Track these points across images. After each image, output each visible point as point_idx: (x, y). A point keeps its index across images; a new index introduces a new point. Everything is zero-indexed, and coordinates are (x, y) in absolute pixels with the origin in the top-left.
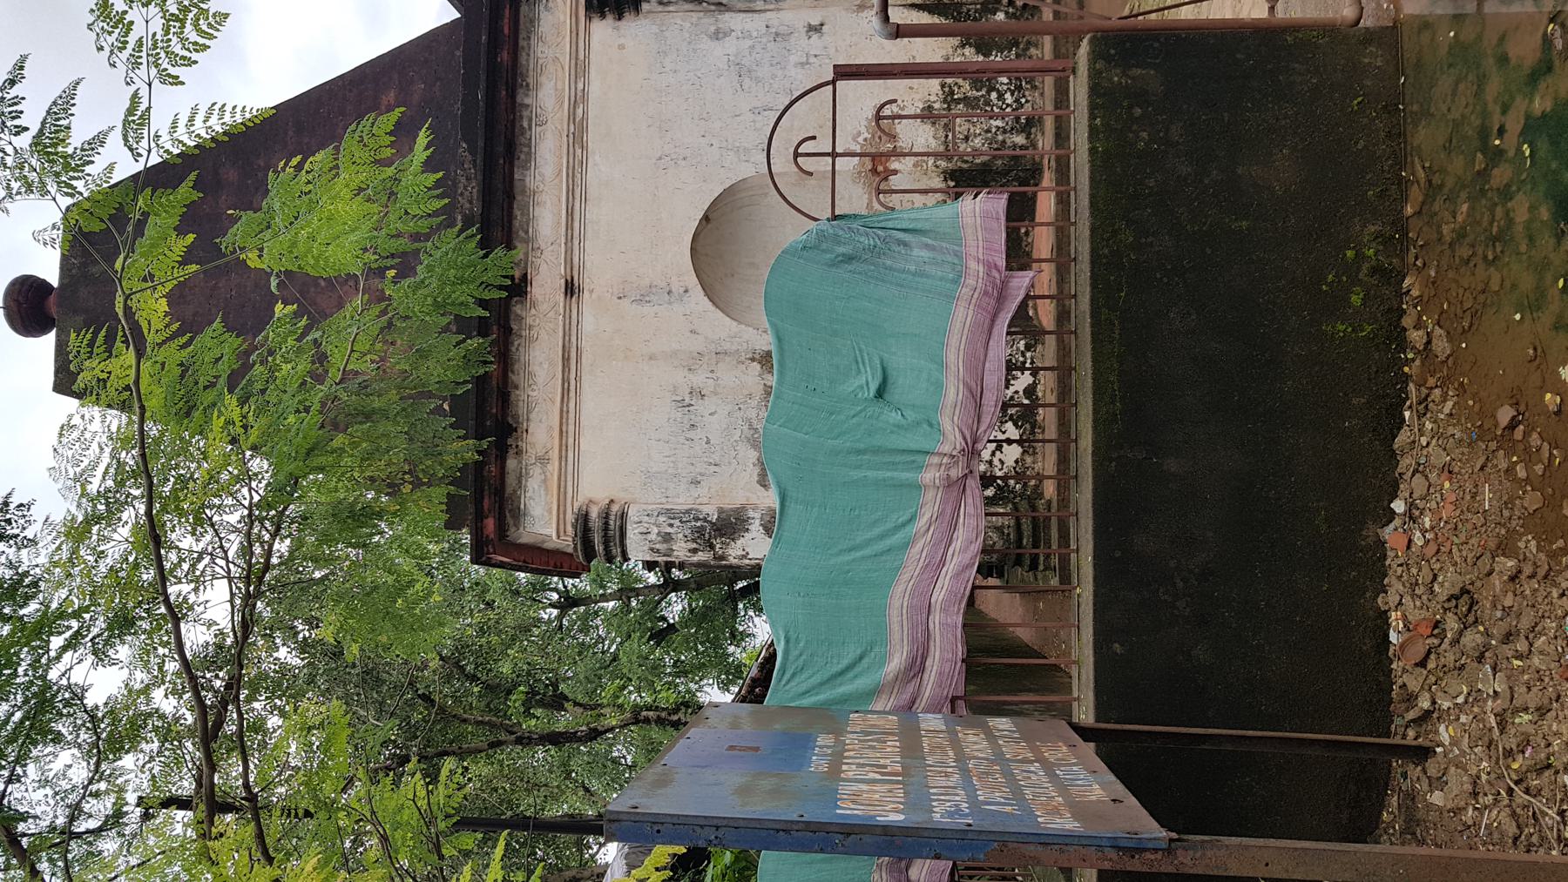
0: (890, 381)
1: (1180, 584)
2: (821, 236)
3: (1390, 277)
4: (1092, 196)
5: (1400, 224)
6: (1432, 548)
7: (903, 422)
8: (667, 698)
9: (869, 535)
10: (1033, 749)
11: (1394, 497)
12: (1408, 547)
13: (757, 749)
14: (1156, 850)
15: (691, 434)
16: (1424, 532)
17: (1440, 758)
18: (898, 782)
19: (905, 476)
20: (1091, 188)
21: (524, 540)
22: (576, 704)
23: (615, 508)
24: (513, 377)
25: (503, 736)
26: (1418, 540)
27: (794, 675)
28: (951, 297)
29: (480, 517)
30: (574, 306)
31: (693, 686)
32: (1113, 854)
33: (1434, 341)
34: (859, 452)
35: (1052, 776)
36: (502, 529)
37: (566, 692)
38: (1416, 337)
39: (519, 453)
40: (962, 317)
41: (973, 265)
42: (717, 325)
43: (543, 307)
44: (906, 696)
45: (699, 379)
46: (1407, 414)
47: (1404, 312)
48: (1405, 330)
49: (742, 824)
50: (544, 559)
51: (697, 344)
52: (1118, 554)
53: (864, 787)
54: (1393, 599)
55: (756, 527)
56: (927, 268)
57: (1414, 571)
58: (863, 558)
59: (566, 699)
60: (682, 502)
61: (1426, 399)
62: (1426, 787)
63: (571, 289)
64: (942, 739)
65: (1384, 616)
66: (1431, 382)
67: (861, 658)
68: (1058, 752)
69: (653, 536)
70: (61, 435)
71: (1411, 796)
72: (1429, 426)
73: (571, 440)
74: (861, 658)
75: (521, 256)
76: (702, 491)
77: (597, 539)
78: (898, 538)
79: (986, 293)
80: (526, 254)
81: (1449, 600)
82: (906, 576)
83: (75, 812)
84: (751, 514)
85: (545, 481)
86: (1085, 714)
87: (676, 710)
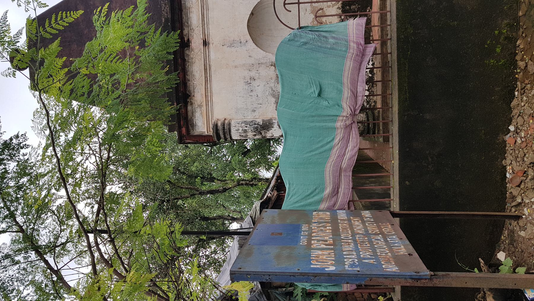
0: (323, 90)
1: (430, 160)
2: (295, 35)
3: (512, 40)
4: (397, 15)
5: (517, 19)
6: (524, 144)
7: (329, 105)
8: (248, 176)
9: (317, 146)
10: (379, 227)
11: (510, 124)
12: (515, 143)
13: (281, 234)
14: (426, 279)
15: (251, 94)
16: (521, 138)
17: (524, 220)
18: (331, 249)
19: (330, 125)
20: (397, 12)
21: (196, 134)
22: (218, 180)
23: (226, 122)
24: (188, 77)
25: (195, 192)
26: (519, 141)
27: (292, 196)
28: (344, 57)
29: (180, 128)
30: (207, 50)
31: (257, 170)
32: (410, 281)
33: (529, 66)
34: (313, 116)
35: (386, 241)
36: (188, 131)
37: (215, 176)
38: (521, 64)
39: (192, 104)
40: (349, 64)
41: (352, 44)
42: (258, 53)
43: (196, 51)
44: (332, 202)
45: (253, 74)
46: (516, 93)
47: (517, 54)
48: (517, 61)
49: (278, 274)
50: (203, 139)
51: (251, 61)
52: (408, 150)
53: (320, 252)
54: (508, 162)
55: (276, 126)
56: (335, 46)
57: (517, 152)
58: (315, 154)
59: (215, 178)
60: (249, 118)
61: (524, 88)
62: (518, 229)
63: (205, 43)
64: (346, 224)
65: (504, 168)
66: (527, 82)
67: (315, 190)
68: (387, 228)
69: (240, 131)
70: (34, 115)
71: (512, 232)
72: (525, 98)
73: (209, 98)
74: (315, 190)
75: (187, 32)
76: (256, 114)
77: (221, 133)
78: (328, 146)
79: (357, 55)
80: (188, 32)
81: (530, 164)
82: (331, 160)
83: (57, 237)
84: (274, 121)
85: (201, 113)
86: (395, 206)
87: (252, 181)
